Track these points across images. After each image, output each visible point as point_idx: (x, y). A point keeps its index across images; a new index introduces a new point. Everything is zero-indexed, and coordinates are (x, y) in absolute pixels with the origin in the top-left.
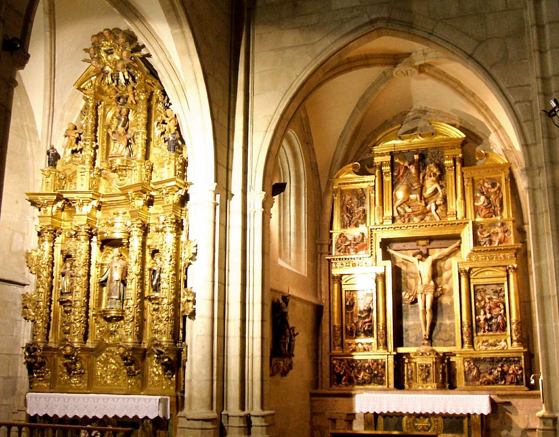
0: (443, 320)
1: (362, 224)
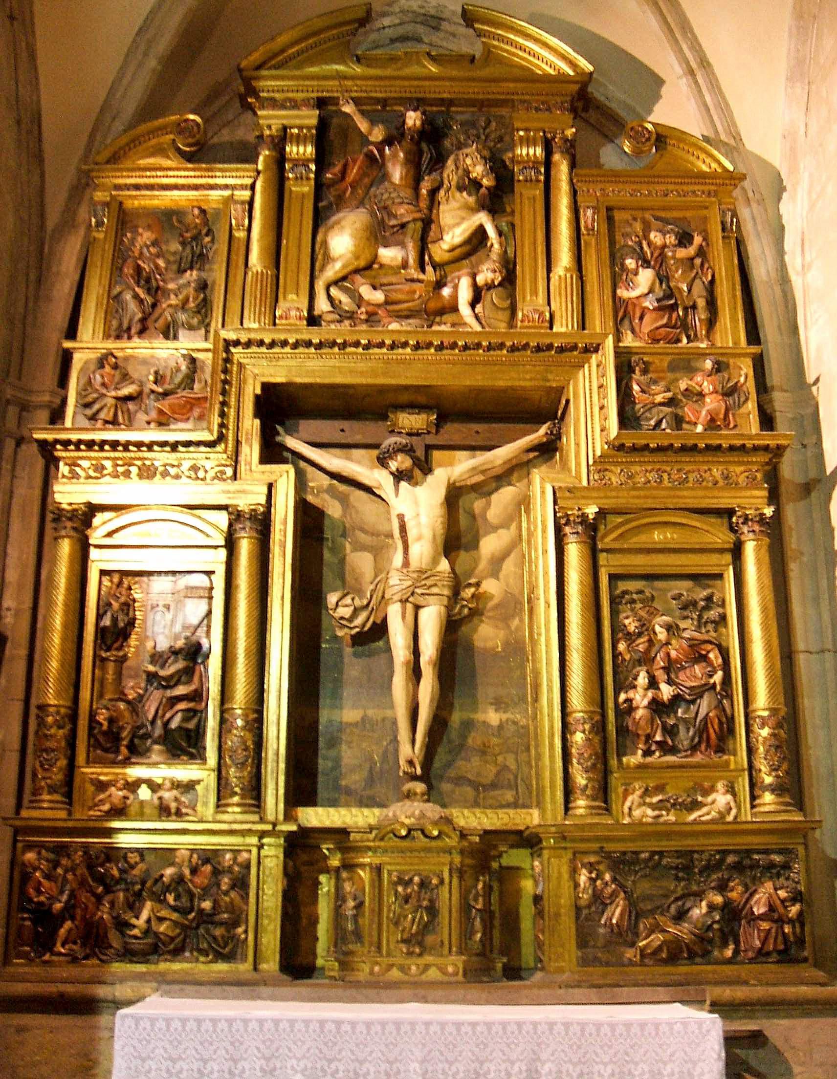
0: (475, 710)
1: (191, 328)
